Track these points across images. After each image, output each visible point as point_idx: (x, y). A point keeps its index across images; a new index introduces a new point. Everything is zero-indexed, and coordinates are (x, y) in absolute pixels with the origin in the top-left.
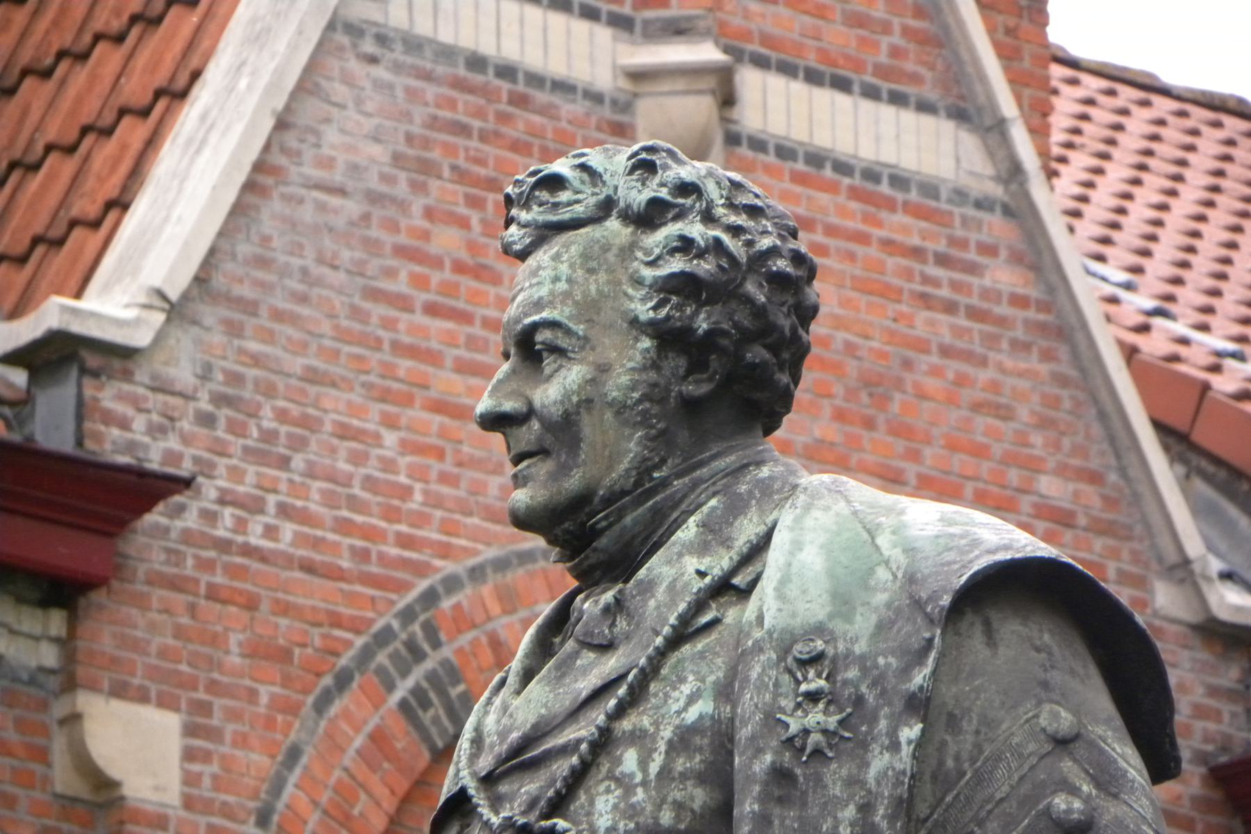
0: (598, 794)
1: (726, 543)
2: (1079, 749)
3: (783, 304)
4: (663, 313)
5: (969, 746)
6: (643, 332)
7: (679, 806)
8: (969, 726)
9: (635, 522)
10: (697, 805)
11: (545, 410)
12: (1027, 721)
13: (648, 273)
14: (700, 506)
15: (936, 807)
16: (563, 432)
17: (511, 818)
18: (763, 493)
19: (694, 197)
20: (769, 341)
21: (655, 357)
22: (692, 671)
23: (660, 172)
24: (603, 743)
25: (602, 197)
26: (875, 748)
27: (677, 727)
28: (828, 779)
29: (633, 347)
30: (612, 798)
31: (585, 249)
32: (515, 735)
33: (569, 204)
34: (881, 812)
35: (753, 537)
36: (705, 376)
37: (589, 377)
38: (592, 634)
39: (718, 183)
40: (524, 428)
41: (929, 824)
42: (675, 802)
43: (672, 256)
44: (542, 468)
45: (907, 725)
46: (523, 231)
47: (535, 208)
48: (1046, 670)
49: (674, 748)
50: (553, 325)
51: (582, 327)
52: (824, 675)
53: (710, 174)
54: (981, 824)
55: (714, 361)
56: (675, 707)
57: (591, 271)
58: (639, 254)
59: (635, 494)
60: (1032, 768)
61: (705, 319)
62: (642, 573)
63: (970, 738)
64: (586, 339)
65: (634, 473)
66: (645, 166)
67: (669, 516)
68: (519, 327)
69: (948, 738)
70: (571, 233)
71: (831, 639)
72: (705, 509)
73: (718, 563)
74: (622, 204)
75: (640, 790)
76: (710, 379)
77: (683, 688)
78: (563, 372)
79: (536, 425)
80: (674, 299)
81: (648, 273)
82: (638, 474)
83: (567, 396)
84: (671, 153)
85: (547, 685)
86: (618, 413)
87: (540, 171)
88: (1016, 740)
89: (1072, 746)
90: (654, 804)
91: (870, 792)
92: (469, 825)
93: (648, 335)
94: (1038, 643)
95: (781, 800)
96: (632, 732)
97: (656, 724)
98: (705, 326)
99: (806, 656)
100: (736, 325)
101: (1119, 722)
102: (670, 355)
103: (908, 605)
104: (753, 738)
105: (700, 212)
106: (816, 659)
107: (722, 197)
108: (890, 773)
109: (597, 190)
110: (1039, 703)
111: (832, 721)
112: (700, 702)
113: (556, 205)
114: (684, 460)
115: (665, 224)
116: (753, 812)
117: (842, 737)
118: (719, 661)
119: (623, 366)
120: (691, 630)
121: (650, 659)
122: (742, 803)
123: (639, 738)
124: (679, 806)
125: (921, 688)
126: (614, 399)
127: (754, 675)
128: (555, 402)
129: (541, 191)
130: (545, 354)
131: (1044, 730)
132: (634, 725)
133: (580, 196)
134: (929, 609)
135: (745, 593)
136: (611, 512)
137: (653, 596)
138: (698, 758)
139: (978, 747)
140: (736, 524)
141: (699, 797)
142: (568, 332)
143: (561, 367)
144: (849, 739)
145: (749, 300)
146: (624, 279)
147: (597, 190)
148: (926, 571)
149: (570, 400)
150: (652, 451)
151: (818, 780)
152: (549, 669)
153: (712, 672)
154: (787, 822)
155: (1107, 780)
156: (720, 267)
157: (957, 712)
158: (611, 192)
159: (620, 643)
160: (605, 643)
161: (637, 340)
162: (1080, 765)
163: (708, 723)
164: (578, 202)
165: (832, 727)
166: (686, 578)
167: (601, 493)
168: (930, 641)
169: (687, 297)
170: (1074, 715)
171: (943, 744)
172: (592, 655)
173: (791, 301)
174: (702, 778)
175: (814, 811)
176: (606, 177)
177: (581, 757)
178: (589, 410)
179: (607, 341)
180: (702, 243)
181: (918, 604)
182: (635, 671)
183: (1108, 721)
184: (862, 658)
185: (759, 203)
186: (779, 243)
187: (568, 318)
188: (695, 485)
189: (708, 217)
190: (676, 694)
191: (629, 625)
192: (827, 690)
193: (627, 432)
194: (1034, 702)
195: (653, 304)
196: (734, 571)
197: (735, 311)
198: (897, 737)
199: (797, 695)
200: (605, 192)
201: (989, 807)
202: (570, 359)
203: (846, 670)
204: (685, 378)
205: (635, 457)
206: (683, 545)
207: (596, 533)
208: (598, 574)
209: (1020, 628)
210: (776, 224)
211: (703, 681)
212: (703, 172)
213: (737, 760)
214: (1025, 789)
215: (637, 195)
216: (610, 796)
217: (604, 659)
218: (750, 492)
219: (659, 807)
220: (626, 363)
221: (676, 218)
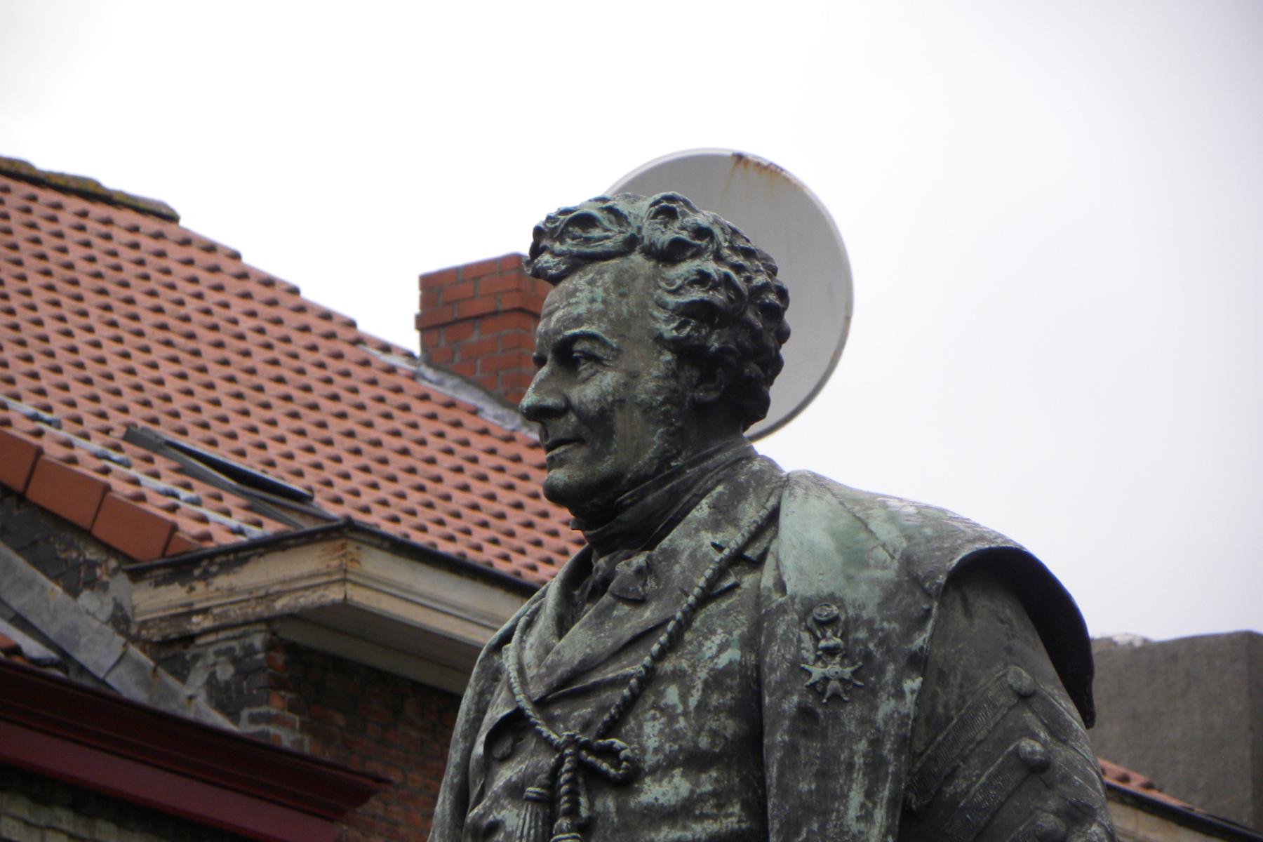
0: (646, 720)
1: (734, 522)
5: (955, 697)
7: (714, 734)
8: (955, 681)
10: (729, 733)
12: (999, 679)
13: (671, 300)
14: (708, 491)
15: (931, 743)
16: (597, 426)
17: (573, 736)
18: (758, 484)
24: (649, 679)
25: (628, 235)
26: (883, 695)
27: (712, 670)
28: (844, 718)
29: (657, 359)
30: (657, 726)
32: (560, 671)
33: (600, 239)
35: (758, 519)
37: (622, 381)
38: (627, 591)
39: (722, 229)
40: (562, 420)
41: (924, 758)
44: (579, 454)
45: (909, 677)
46: (557, 260)
47: (569, 241)
53: (716, 222)
54: (965, 760)
56: (708, 654)
57: (623, 295)
58: (663, 284)
60: (1004, 716)
61: (717, 340)
62: (665, 542)
63: (956, 691)
64: (619, 351)
65: (656, 461)
68: (559, 337)
69: (939, 689)
70: (602, 263)
71: (840, 602)
72: (715, 493)
73: (733, 538)
74: (646, 242)
75: (681, 719)
77: (714, 638)
78: (599, 377)
80: (693, 322)
81: (671, 300)
83: (603, 395)
84: (687, 203)
85: (590, 629)
86: (644, 412)
88: (991, 694)
90: (694, 731)
91: (878, 730)
92: (521, 739)
93: (669, 350)
95: (805, 733)
96: (674, 672)
97: (693, 666)
98: (717, 345)
99: (821, 618)
100: (739, 345)
101: (1060, 683)
104: (781, 683)
105: (712, 252)
106: (833, 621)
108: (896, 716)
109: (623, 229)
110: (1006, 665)
112: (730, 650)
113: (588, 240)
115: (684, 260)
116: (784, 742)
117: (855, 685)
118: (742, 618)
119: (650, 374)
120: (715, 591)
121: (684, 613)
122: (773, 734)
123: (678, 676)
124: (714, 734)
125: (921, 649)
127: (780, 631)
128: (593, 401)
130: (582, 361)
131: (1011, 686)
132: (675, 666)
133: (608, 234)
135: (757, 564)
137: (677, 562)
138: (729, 696)
140: (740, 506)
141: (730, 727)
142: (604, 344)
143: (597, 372)
145: (749, 326)
146: (650, 303)
147: (623, 229)
148: (922, 555)
149: (606, 400)
151: (836, 718)
154: (811, 751)
158: (634, 231)
161: (660, 353)
162: (1037, 716)
163: (737, 668)
164: (607, 238)
165: (847, 677)
166: (704, 549)
168: (928, 613)
171: (935, 694)
172: (627, 608)
174: (732, 712)
176: (631, 219)
177: (631, 689)
178: (621, 408)
179: (636, 353)
181: (916, 581)
184: (870, 622)
187: (605, 332)
188: (704, 472)
189: (718, 258)
190: (708, 644)
191: (658, 584)
193: (651, 428)
195: (675, 325)
196: (746, 546)
198: (902, 687)
199: (817, 649)
200: (631, 231)
201: (971, 747)
202: (605, 366)
204: (696, 386)
206: (699, 522)
207: (622, 508)
208: (319, 536)
209: (988, 603)
211: (731, 634)
212: (711, 220)
213: (767, 699)
215: (664, 236)
216: (656, 723)
217: (638, 611)
218: (748, 482)
219: (698, 733)
220: (654, 373)
221: (694, 256)
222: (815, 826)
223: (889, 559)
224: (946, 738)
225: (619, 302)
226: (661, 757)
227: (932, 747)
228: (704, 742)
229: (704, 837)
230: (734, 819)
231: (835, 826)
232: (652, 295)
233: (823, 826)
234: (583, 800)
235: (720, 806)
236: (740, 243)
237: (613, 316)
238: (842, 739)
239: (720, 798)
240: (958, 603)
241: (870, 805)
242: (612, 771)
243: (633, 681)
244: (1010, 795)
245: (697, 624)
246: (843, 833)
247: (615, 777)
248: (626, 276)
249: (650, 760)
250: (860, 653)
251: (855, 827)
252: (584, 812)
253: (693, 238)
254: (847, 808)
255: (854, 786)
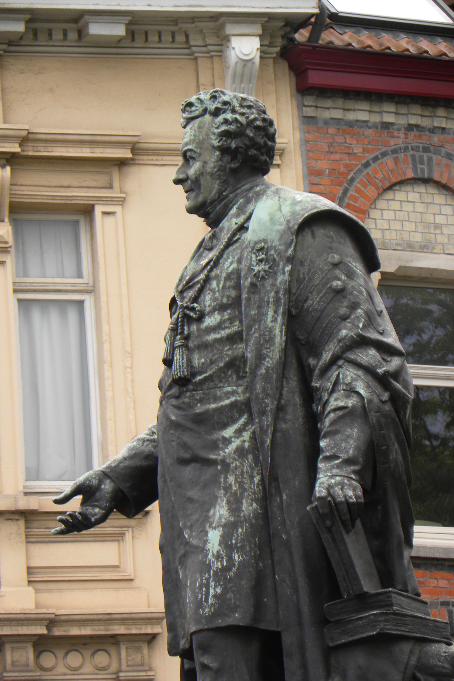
2: (341, 266)
3: (260, 135)
4: (221, 143)
5: (307, 270)
7: (228, 297)
8: (306, 264)
12: (325, 260)
13: (216, 131)
24: (207, 280)
25: (204, 107)
26: (279, 274)
27: (227, 273)
28: (266, 285)
30: (210, 296)
33: (195, 111)
34: (281, 293)
39: (237, 100)
40: (187, 183)
41: (296, 295)
42: (227, 295)
47: (186, 113)
48: (331, 243)
49: (226, 279)
50: (190, 150)
55: (239, 156)
60: (326, 274)
62: (221, 225)
63: (307, 268)
64: (200, 154)
65: (217, 194)
69: (301, 268)
72: (239, 203)
73: (241, 219)
75: (217, 293)
76: (238, 162)
78: (195, 164)
79: (189, 182)
80: (224, 138)
83: (196, 172)
86: (211, 176)
88: (321, 266)
89: (339, 266)
91: (278, 287)
94: (328, 235)
95: (253, 293)
97: (221, 272)
99: (261, 248)
100: (244, 144)
102: (226, 156)
104: (246, 274)
106: (262, 249)
110: (329, 254)
111: (267, 267)
113: (191, 112)
117: (270, 272)
119: (211, 161)
120: (232, 242)
123: (217, 277)
124: (228, 297)
125: (290, 255)
131: (330, 262)
133: (197, 108)
134: (292, 230)
138: (233, 281)
139: (310, 270)
140: (248, 206)
141: (233, 293)
142: (195, 152)
144: (271, 272)
145: (247, 136)
149: (197, 173)
151: (263, 286)
154: (256, 299)
155: (351, 275)
157: (303, 260)
158: (206, 106)
161: (215, 152)
163: (235, 271)
164: (197, 110)
168: (292, 240)
169: (228, 137)
170: (340, 256)
171: (299, 270)
172: (207, 252)
173: (263, 133)
175: (262, 295)
176: (205, 101)
177: (201, 285)
178: (203, 176)
180: (231, 120)
182: (215, 257)
183: (351, 256)
186: (257, 116)
187: (195, 148)
188: (236, 195)
189: (234, 111)
190: (227, 263)
193: (214, 181)
194: (327, 254)
199: (257, 260)
200: (204, 106)
201: (313, 287)
202: (196, 160)
204: (231, 162)
211: (234, 258)
214: (324, 281)
215: (212, 107)
218: (253, 196)
219: (223, 297)
220: (212, 159)
222: (257, 327)
224: (304, 286)
225: (199, 135)
226: (211, 308)
227: (299, 290)
228: (225, 300)
229: (225, 335)
230: (236, 327)
231: (263, 326)
232: (211, 130)
233: (259, 326)
234: (186, 328)
235: (231, 323)
236: (246, 104)
238: (265, 293)
239: (231, 320)
241: (276, 316)
242: (194, 316)
243: (202, 281)
244: (328, 303)
245: (225, 256)
246: (266, 328)
247: (195, 318)
248: (202, 124)
249: (208, 309)
250: (272, 260)
251: (270, 325)
252: (186, 332)
253: (222, 106)
254: (267, 318)
255: (270, 310)
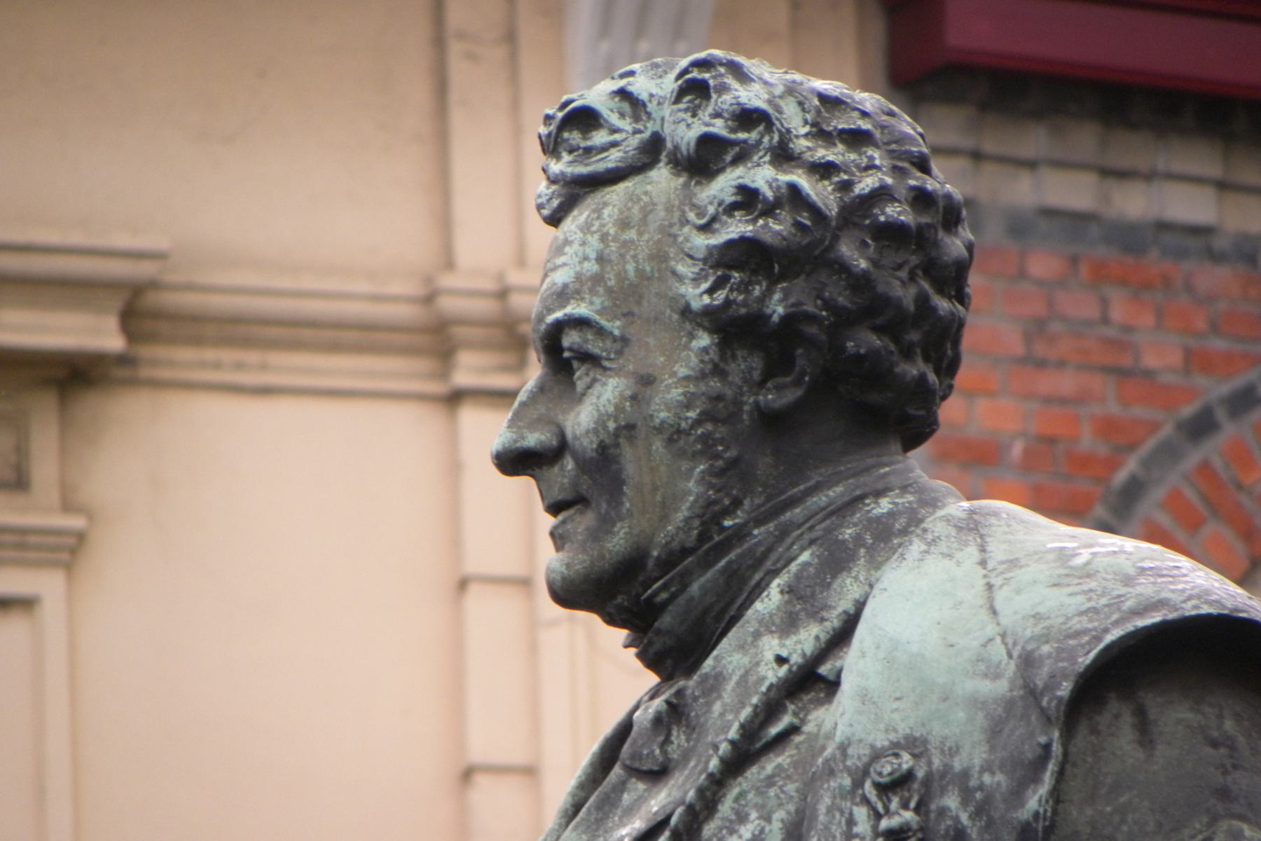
3: (900, 267)
4: (721, 296)
6: (700, 325)
9: (704, 591)
11: (577, 443)
13: (702, 242)
19: (761, 128)
20: (879, 321)
21: (716, 359)
22: (756, 806)
23: (714, 96)
25: (647, 135)
29: (687, 347)
31: (621, 212)
36: (788, 379)
37: (628, 393)
40: (556, 469)
43: (731, 216)
46: (554, 187)
47: (566, 157)
50: (580, 323)
51: (618, 323)
52: (913, 804)
59: (700, 552)
61: (781, 301)
64: (624, 340)
65: (696, 523)
66: (694, 90)
67: (750, 577)
68: (543, 327)
72: (794, 567)
73: (806, 640)
74: (669, 145)
76: (797, 383)
78: (597, 388)
79: (569, 464)
82: (703, 524)
83: (601, 421)
85: (584, 832)
86: (670, 441)
87: (572, 101)
93: (705, 329)
94: (1215, 734)
98: (780, 310)
100: (828, 305)
102: (739, 353)
103: (1022, 697)
106: (900, 782)
107: (806, 122)
110: (1214, 820)
113: (588, 151)
114: (769, 499)
115: (721, 170)
119: (674, 374)
120: (758, 745)
125: (1036, 815)
126: (663, 422)
128: (588, 432)
129: (570, 131)
130: (575, 364)
133: (617, 137)
134: (1044, 703)
136: (672, 579)
140: (835, 585)
142: (601, 332)
143: (595, 380)
145: (843, 268)
147: (640, 126)
149: (605, 428)
150: (719, 490)
152: (589, 810)
153: (780, 805)
156: (799, 226)
158: (657, 128)
159: (674, 768)
160: (656, 768)
161: (692, 336)
164: (614, 144)
167: (655, 553)
168: (1047, 747)
172: (641, 786)
173: (914, 260)
176: (651, 107)
178: (631, 439)
179: (651, 341)
180: (770, 194)
182: (680, 810)
185: (865, 125)
187: (599, 312)
188: (784, 533)
189: (783, 155)
191: (688, 740)
192: (915, 826)
193: (685, 466)
194: (1205, 820)
197: (825, 285)
200: (651, 127)
202: (605, 369)
203: (942, 795)
204: (762, 384)
205: (696, 501)
206: (761, 622)
209: (1190, 716)
210: (891, 152)
211: (768, 819)
212: (779, 90)
215: (686, 131)
218: (858, 539)
221: (737, 161)
223: (1005, 657)
237: (612, 283)
240: (1127, 719)
